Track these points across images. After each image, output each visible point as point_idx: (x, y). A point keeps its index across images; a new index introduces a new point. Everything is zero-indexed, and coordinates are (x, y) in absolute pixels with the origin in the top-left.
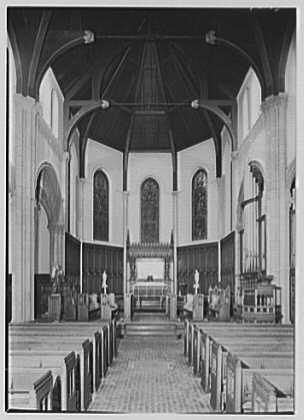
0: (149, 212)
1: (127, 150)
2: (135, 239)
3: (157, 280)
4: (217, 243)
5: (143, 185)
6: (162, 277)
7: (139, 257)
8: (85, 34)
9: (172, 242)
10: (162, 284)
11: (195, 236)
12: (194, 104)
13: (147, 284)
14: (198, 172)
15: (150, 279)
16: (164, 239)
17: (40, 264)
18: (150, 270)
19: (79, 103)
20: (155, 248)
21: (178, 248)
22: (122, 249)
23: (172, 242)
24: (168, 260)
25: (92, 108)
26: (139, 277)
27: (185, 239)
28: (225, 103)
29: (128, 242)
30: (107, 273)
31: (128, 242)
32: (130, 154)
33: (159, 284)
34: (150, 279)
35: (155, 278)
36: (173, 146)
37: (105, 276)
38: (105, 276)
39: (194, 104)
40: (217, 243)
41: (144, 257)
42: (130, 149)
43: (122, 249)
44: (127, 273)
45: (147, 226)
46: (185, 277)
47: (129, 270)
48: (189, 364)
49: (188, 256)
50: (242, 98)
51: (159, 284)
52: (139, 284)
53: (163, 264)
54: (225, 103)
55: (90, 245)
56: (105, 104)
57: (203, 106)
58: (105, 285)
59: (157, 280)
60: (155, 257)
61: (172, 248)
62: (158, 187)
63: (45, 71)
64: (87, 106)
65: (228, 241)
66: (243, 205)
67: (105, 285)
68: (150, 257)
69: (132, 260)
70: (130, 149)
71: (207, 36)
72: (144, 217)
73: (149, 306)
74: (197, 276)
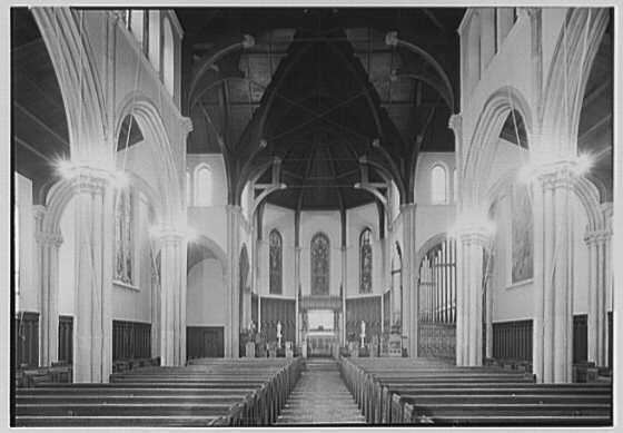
0: (320, 265)
1: (299, 207)
2: (306, 292)
3: (327, 330)
4: (380, 298)
5: (313, 241)
6: (332, 327)
7: (311, 308)
8: (244, 39)
9: (341, 294)
10: (332, 334)
11: (362, 288)
12: (357, 186)
13: (320, 333)
14: (363, 232)
15: (321, 329)
16: (334, 291)
17: (16, 199)
18: (321, 321)
19: (262, 186)
20: (326, 300)
21: (347, 301)
22: (294, 302)
23: (341, 294)
24: (337, 311)
25: (284, 245)
26: (311, 326)
27: (353, 293)
28: (381, 186)
29: (300, 294)
30: (282, 324)
31: (300, 294)
32: (302, 213)
33: (329, 334)
34: (321, 329)
35: (325, 327)
36: (341, 203)
37: (279, 326)
38: (279, 326)
39: (357, 186)
40: (380, 298)
41: (315, 308)
42: (302, 209)
43: (294, 302)
44: (299, 324)
45: (317, 278)
46: (353, 327)
47: (301, 321)
48: (359, 408)
49: (356, 309)
50: (467, 27)
51: (329, 334)
52: (311, 334)
53: (333, 315)
54: (381, 186)
55: (268, 299)
56: (284, 186)
57: (364, 187)
58: (279, 335)
59: (327, 330)
60: (325, 308)
61: (342, 300)
62: (328, 242)
63: (243, 188)
64: (268, 189)
65: (387, 296)
66: (393, 273)
67: (279, 335)
68: (320, 308)
69: (304, 311)
70: (303, 205)
71: (387, 37)
72: (315, 270)
73: (321, 350)
74: (363, 325)
